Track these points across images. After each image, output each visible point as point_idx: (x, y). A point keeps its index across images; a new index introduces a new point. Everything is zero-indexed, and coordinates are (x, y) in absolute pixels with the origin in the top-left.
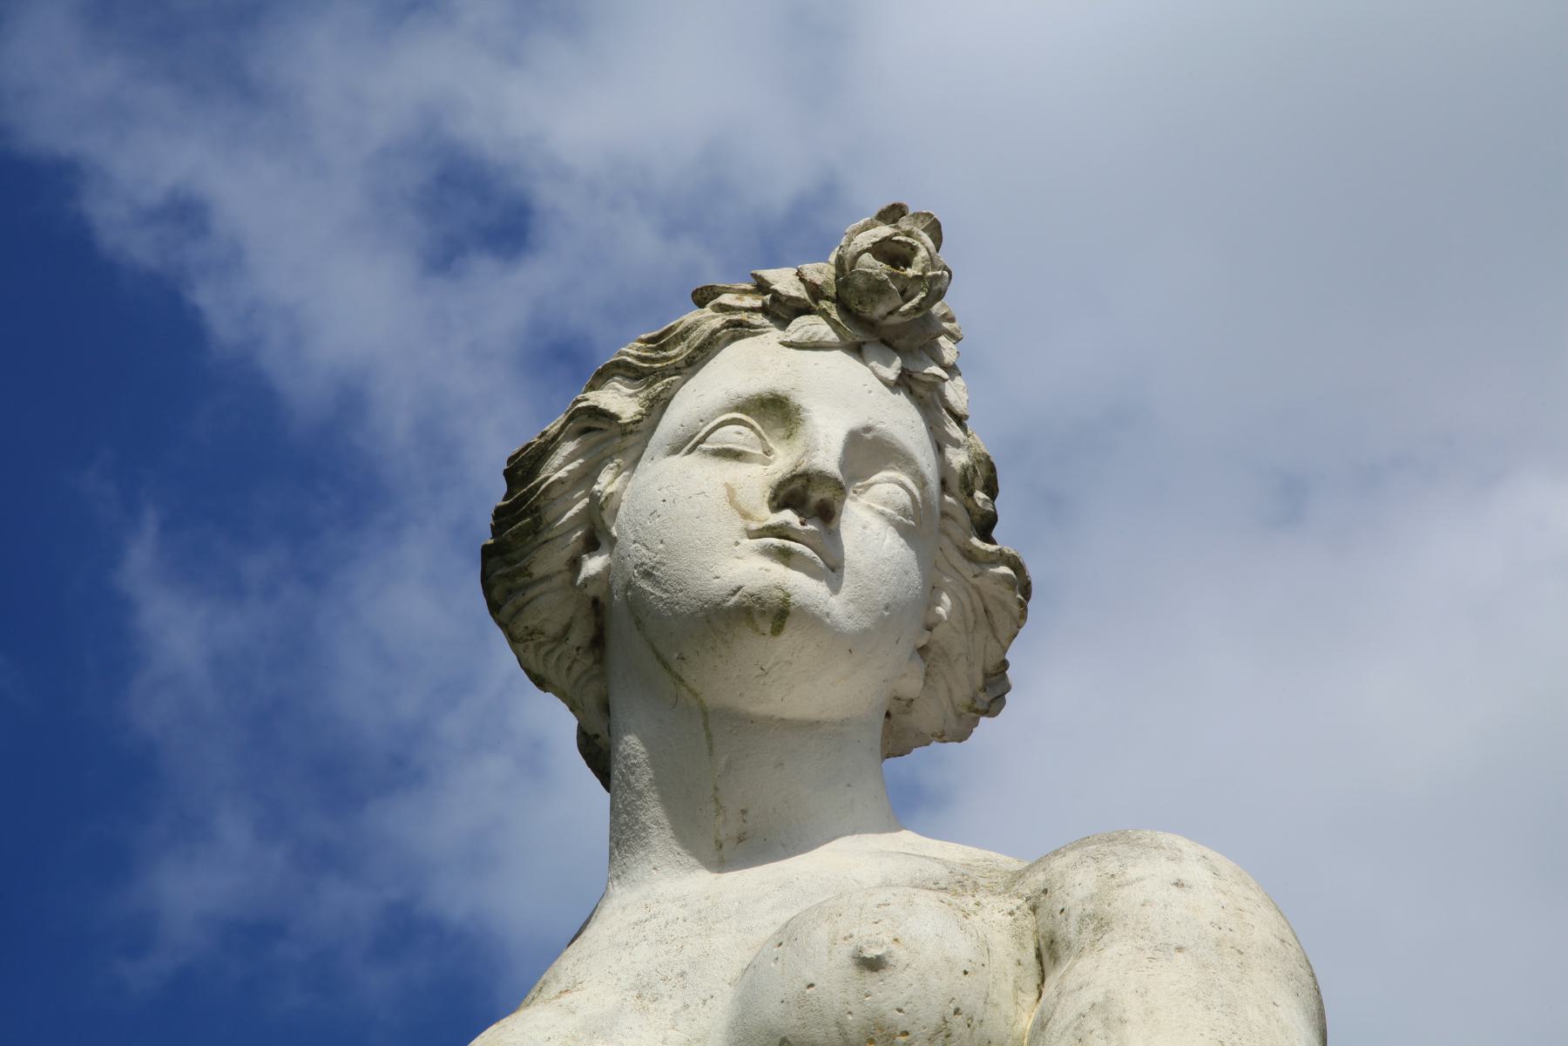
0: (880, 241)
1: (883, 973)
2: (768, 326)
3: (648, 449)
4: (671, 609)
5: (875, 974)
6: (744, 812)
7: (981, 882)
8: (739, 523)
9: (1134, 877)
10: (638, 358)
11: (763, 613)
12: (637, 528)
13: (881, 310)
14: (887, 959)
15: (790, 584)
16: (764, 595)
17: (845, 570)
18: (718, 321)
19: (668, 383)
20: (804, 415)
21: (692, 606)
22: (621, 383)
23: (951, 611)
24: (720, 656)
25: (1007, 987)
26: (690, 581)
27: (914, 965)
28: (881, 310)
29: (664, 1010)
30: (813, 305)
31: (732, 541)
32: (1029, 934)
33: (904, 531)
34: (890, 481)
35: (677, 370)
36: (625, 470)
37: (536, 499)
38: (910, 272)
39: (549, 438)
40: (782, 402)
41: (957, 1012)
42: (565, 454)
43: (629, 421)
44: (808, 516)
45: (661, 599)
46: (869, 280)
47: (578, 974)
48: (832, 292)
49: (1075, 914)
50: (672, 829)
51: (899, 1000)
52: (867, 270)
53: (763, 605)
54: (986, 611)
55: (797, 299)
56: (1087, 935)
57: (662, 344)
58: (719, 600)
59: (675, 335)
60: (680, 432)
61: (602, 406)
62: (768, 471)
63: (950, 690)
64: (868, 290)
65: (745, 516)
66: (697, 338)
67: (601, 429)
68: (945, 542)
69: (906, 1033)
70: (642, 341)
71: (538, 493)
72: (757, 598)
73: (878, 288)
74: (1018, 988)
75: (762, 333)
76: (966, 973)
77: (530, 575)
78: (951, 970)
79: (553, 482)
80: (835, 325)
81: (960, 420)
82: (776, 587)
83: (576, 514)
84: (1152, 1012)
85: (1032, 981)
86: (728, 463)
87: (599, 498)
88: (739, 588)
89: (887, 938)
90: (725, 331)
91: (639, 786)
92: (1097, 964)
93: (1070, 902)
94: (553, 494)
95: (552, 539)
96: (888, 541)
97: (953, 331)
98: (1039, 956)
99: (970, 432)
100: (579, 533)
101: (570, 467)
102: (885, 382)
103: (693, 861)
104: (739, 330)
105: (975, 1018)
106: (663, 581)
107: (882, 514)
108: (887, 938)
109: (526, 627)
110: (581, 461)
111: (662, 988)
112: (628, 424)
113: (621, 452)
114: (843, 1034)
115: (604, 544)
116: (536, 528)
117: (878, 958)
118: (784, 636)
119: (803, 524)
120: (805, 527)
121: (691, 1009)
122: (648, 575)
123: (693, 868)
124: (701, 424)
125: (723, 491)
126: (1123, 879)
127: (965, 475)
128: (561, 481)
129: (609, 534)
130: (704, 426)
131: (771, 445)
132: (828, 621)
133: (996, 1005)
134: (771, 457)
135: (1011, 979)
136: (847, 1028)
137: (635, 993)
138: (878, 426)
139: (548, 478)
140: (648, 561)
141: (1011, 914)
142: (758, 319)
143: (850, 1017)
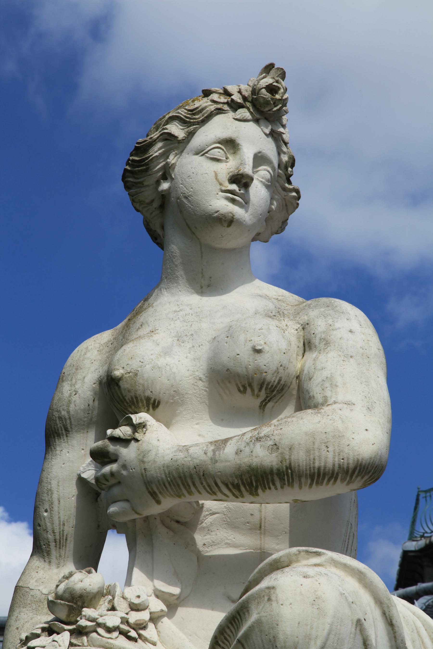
0: (269, 85)
1: (261, 354)
2: (229, 111)
3: (186, 149)
4: (194, 212)
5: (259, 354)
6: (210, 278)
7: (286, 312)
8: (219, 187)
9: (337, 327)
10: (185, 116)
11: (225, 221)
12: (183, 179)
13: (267, 109)
14: (263, 350)
15: (235, 212)
16: (226, 215)
17: (250, 204)
18: (213, 107)
19: (195, 128)
20: (240, 147)
21: (201, 213)
22: (178, 124)
23: (276, 207)
24: (209, 230)
25: (295, 356)
26: (201, 205)
27: (270, 352)
28: (267, 109)
29: (186, 346)
30: (244, 104)
31: (216, 193)
32: (302, 337)
33: (267, 187)
34: (265, 170)
35: (198, 123)
36: (178, 155)
37: (148, 162)
38: (278, 97)
39: (153, 140)
40: (233, 142)
41: (281, 366)
42: (158, 147)
43: (181, 139)
44: (241, 187)
45: (191, 208)
46: (264, 100)
47: (156, 325)
48: (250, 99)
49: (318, 336)
50: (187, 279)
51: (265, 362)
52: (264, 96)
53: (225, 218)
54: (286, 205)
55: (240, 103)
56: (322, 346)
57: (194, 113)
58: (211, 213)
59: (198, 111)
60: (199, 148)
61: (172, 133)
62: (228, 167)
63: (271, 229)
64: (264, 103)
65: (221, 184)
66: (206, 113)
67: (171, 140)
68: (277, 184)
69: (266, 372)
70: (186, 109)
71: (149, 159)
72: (224, 215)
73: (267, 103)
74: (297, 355)
75: (227, 113)
76: (284, 353)
77: (143, 184)
78: (280, 353)
79: (154, 157)
80: (251, 113)
81: (286, 144)
82: (230, 213)
83: (160, 167)
84: (345, 384)
85: (301, 353)
86: (215, 163)
87: (169, 164)
88: (218, 211)
89: (262, 342)
90: (215, 111)
91: (176, 263)
92: (326, 360)
93: (316, 332)
94: (154, 160)
95: (152, 174)
96: (263, 191)
97: (286, 110)
98: (304, 344)
99: (288, 147)
100: (160, 174)
101: (160, 152)
102: (266, 134)
103: (193, 291)
104: (219, 111)
105: (286, 367)
106: (192, 202)
107: (261, 182)
108: (262, 342)
109: (139, 200)
110: (163, 150)
111: (186, 339)
112: (181, 140)
113: (176, 148)
114: (247, 371)
115: (169, 178)
116: (147, 170)
117: (260, 349)
118: (231, 228)
119: (240, 190)
120: (240, 192)
121: (195, 348)
122: (186, 198)
123: (193, 293)
124: (206, 147)
125: (213, 174)
126: (334, 327)
127: (286, 165)
128: (157, 156)
129: (171, 176)
130: (207, 147)
131: (228, 155)
132: (244, 223)
133: (292, 362)
134: (228, 160)
135: (296, 352)
136: (249, 369)
137: (177, 339)
138: (263, 151)
139: (152, 155)
140: (186, 193)
141: (297, 330)
142: (226, 107)
143: (250, 366)
